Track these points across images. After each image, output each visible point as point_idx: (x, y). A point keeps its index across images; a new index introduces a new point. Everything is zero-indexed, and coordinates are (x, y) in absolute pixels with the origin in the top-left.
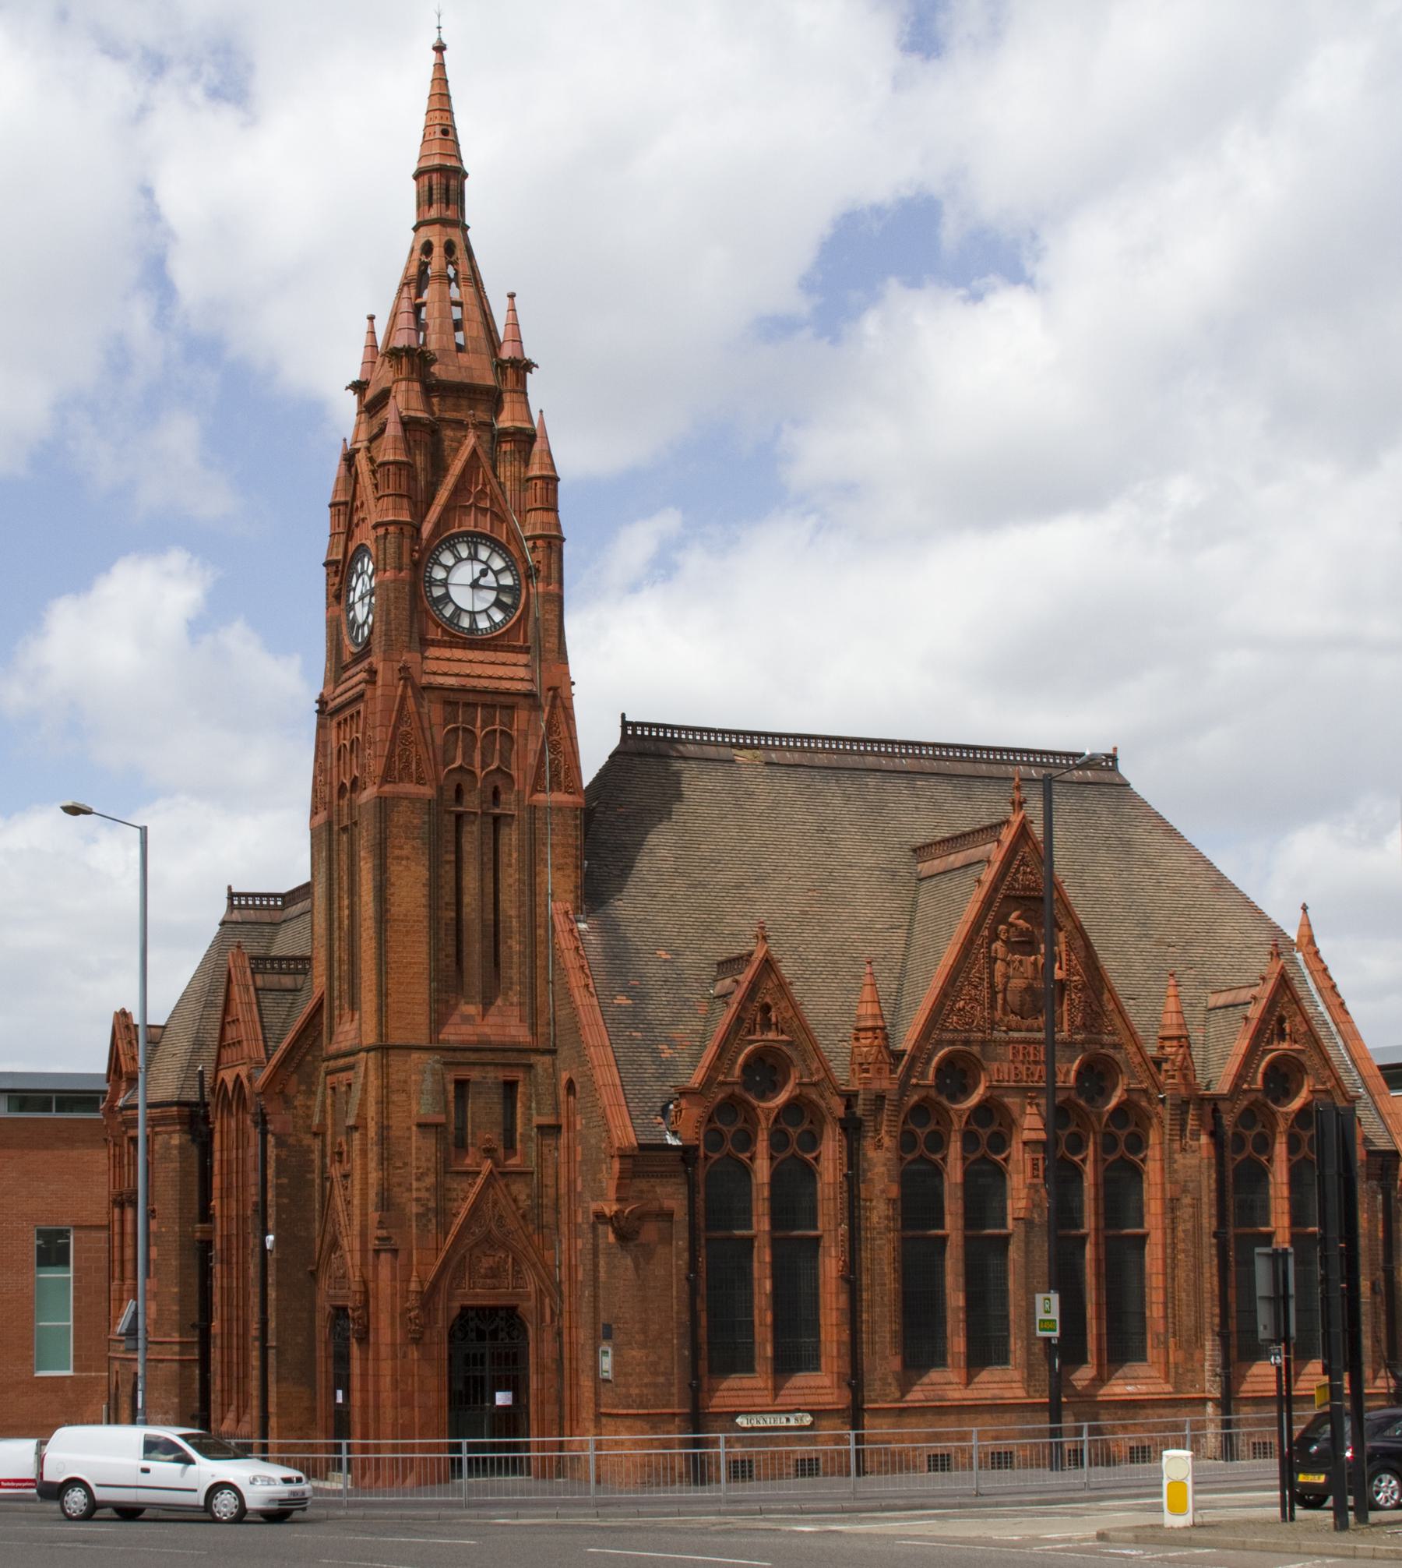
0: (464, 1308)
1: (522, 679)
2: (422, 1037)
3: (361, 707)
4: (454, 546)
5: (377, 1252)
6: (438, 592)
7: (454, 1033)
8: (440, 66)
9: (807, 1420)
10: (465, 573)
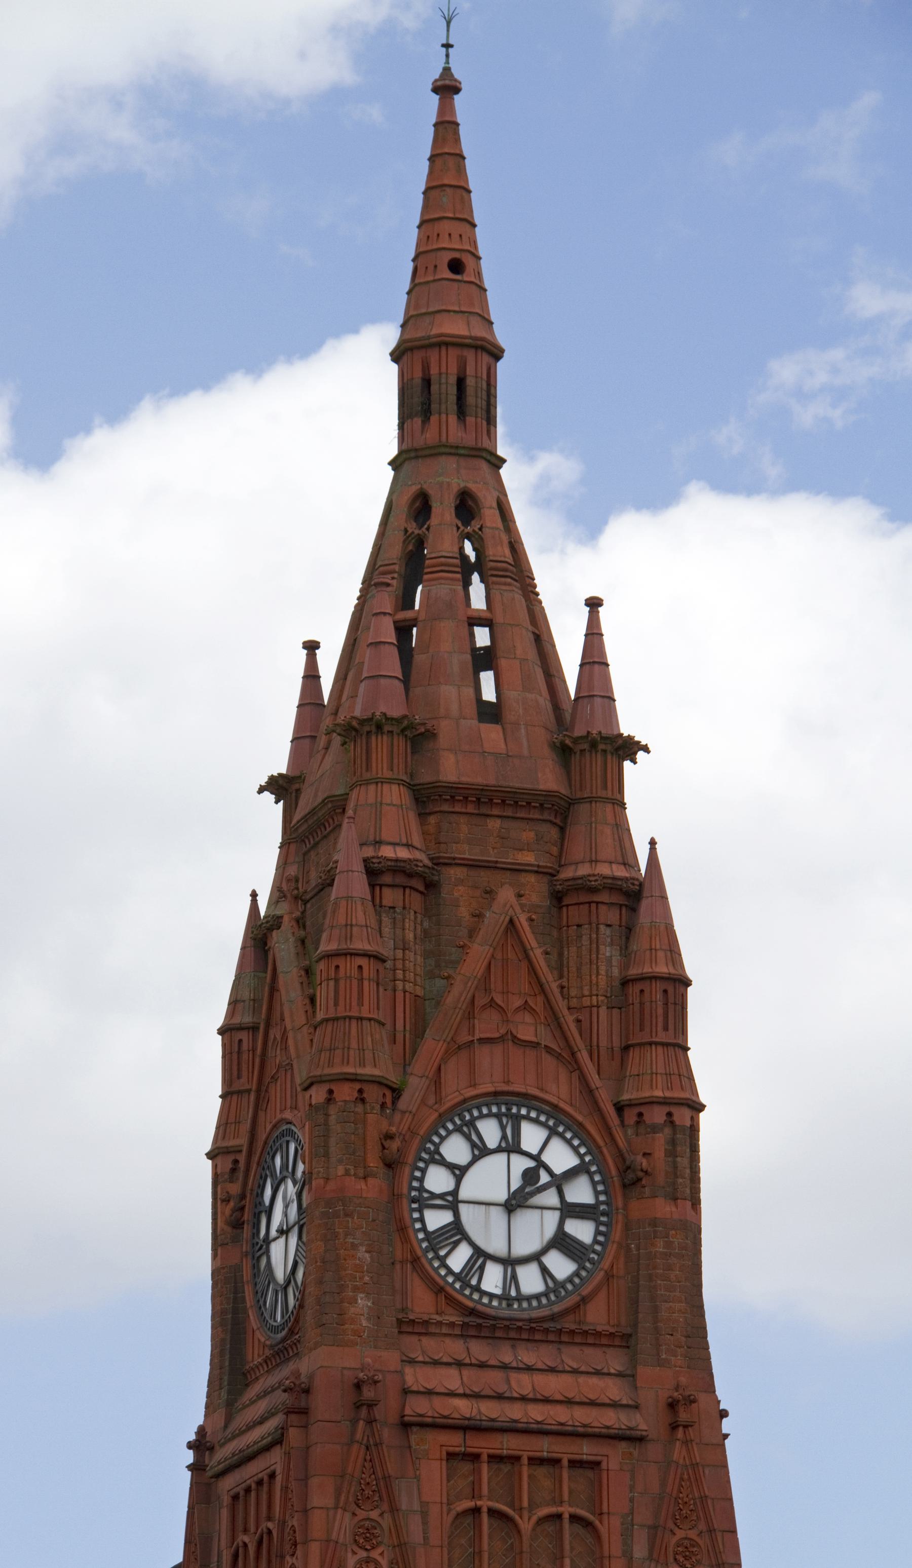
1: (614, 1405)
3: (275, 1459)
4: (472, 1124)
8: (446, 128)
10: (491, 1179)
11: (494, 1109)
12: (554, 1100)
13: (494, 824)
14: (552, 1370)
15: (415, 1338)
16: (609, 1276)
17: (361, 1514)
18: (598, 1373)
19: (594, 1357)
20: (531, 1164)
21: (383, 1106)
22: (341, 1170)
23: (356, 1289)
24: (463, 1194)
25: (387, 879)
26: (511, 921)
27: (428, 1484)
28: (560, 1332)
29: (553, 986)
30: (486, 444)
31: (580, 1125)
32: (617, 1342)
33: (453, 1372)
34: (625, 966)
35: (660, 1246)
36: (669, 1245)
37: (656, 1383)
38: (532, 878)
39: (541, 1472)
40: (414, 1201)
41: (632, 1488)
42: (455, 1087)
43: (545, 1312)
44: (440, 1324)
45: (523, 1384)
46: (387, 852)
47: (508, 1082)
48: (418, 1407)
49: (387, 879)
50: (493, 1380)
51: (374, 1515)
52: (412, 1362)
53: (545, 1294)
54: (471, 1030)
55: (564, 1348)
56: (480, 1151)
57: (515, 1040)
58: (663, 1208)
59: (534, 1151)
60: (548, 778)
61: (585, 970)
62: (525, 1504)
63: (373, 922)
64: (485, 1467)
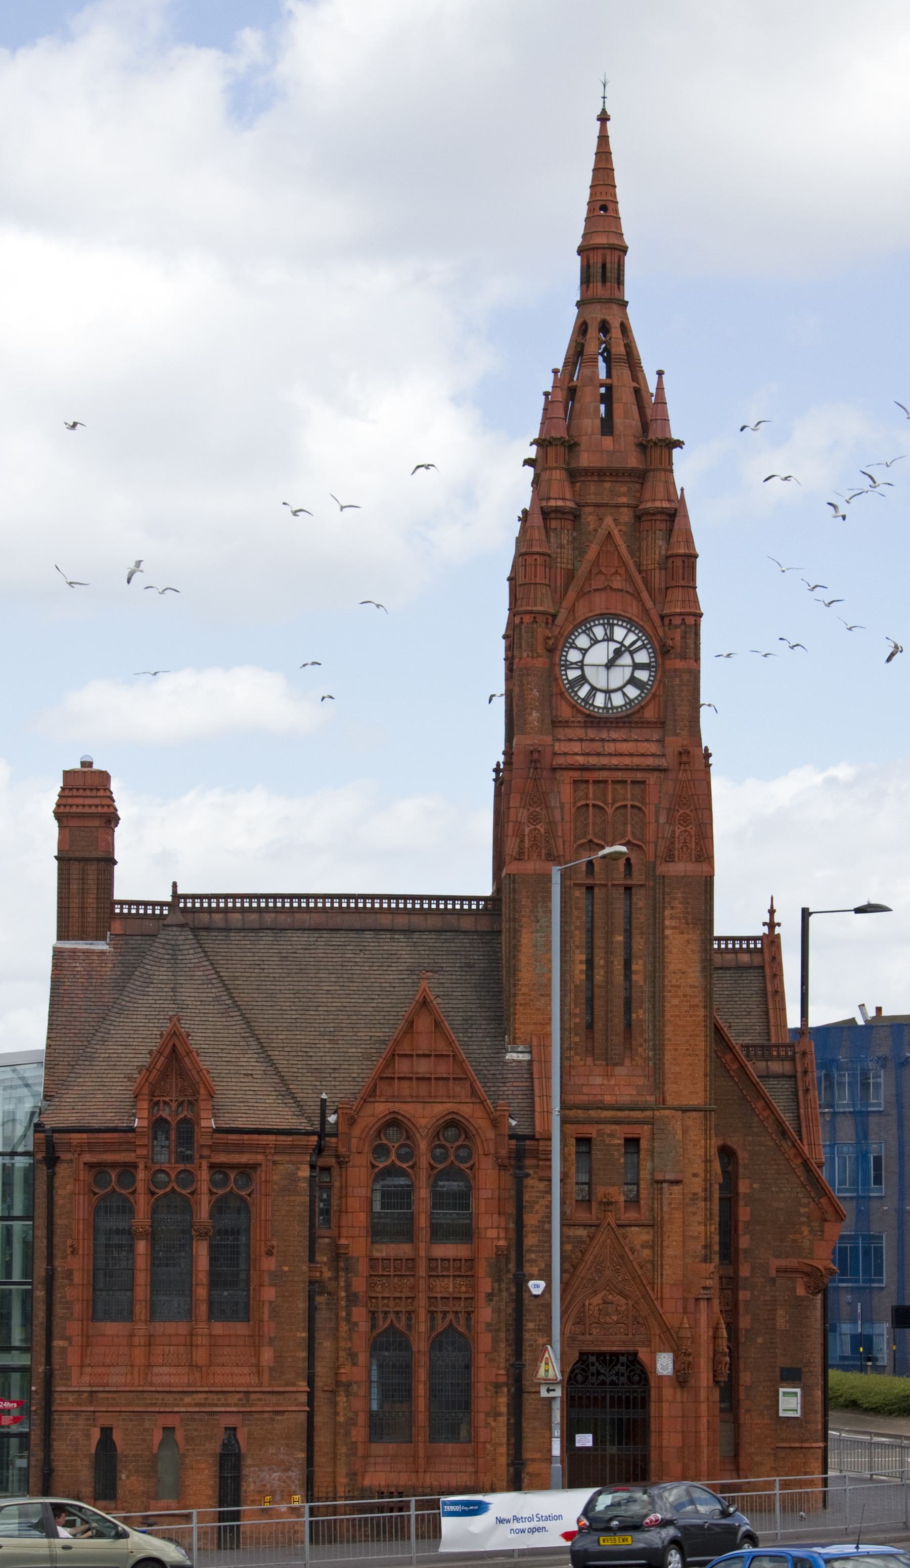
1: (653, 755)
4: (590, 629)
8: (603, 139)
10: (600, 654)
11: (601, 622)
12: (629, 615)
13: (607, 485)
14: (625, 740)
15: (561, 729)
16: (654, 696)
17: (532, 809)
18: (647, 740)
19: (646, 733)
20: (619, 646)
21: (547, 623)
22: (525, 655)
23: (532, 709)
24: (586, 662)
25: (553, 515)
26: (609, 533)
27: (564, 793)
28: (630, 722)
29: (630, 562)
30: (617, 295)
31: (642, 627)
32: (659, 725)
33: (578, 744)
34: (667, 551)
35: (677, 681)
36: (682, 680)
37: (674, 743)
38: (625, 510)
39: (618, 786)
40: (563, 666)
41: (660, 792)
42: (582, 611)
43: (624, 714)
44: (573, 722)
45: (610, 748)
46: (552, 503)
47: (607, 609)
48: (560, 761)
49: (553, 515)
50: (597, 747)
51: (538, 809)
52: (559, 740)
53: (625, 705)
54: (590, 586)
55: (633, 730)
56: (595, 642)
57: (611, 588)
59: (620, 640)
60: (633, 461)
61: (649, 552)
62: (610, 801)
63: (544, 537)
64: (591, 786)
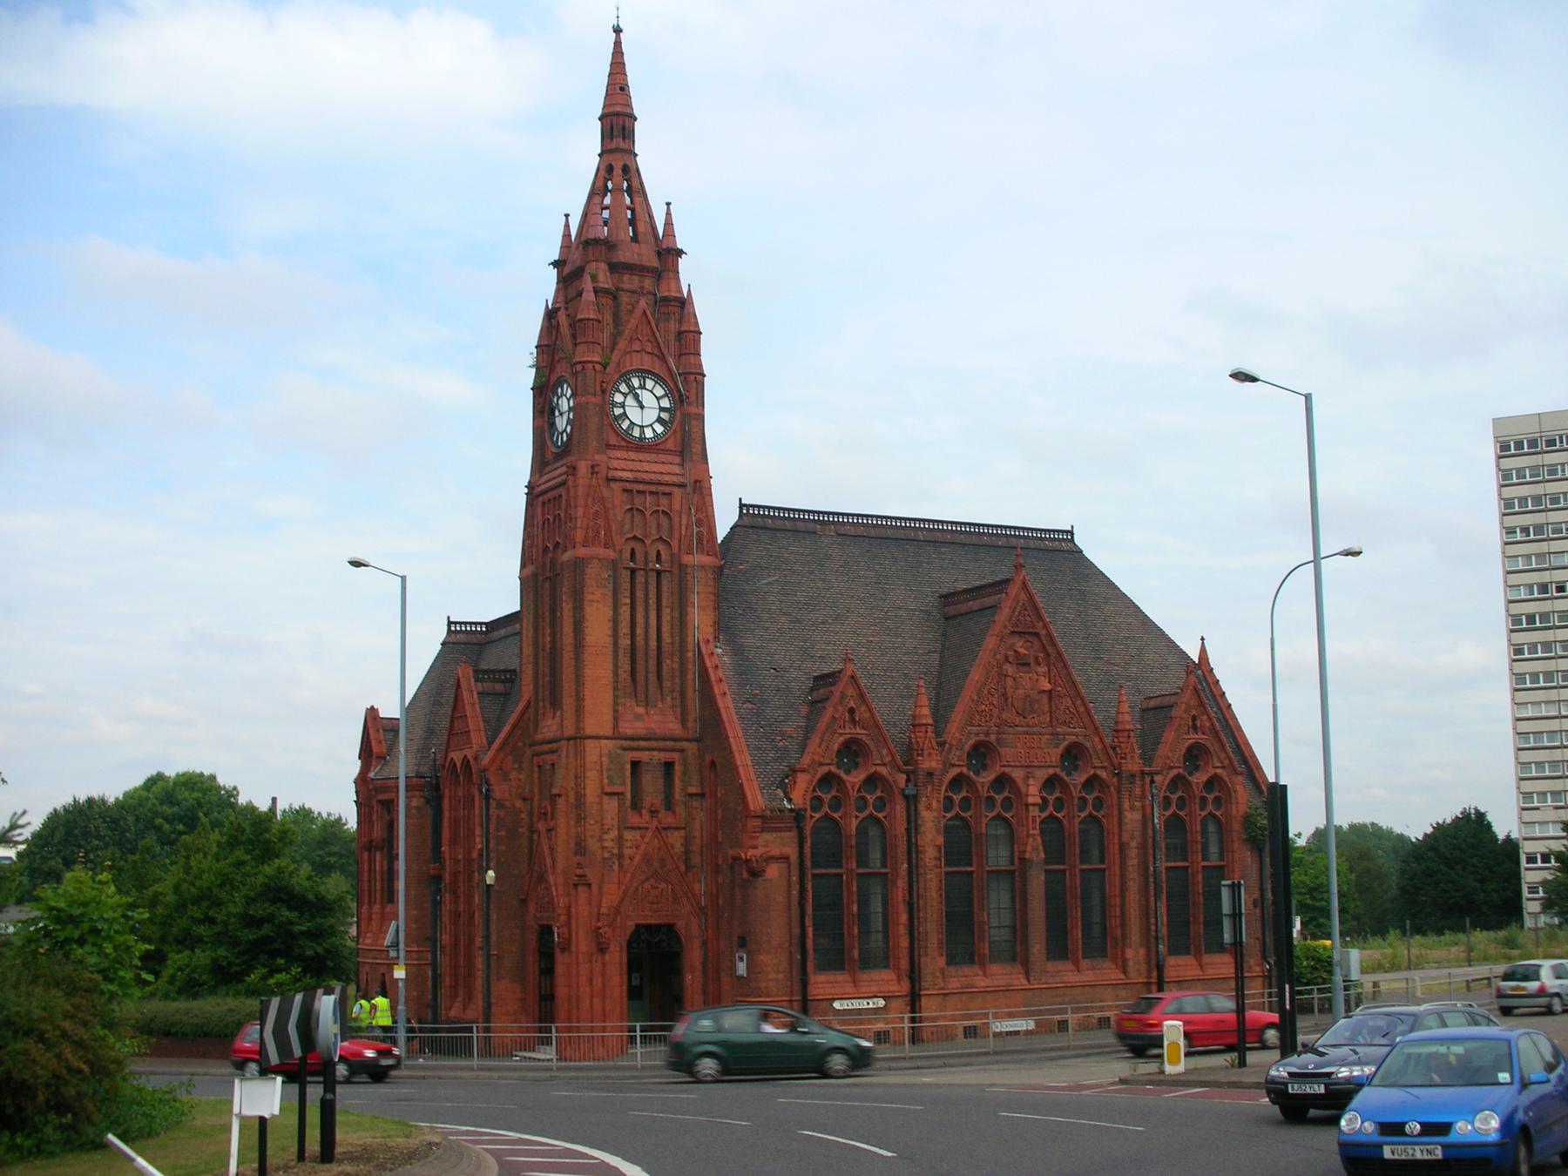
0: (637, 926)
2: (608, 731)
3: (562, 491)
5: (576, 885)
6: (618, 411)
7: (627, 728)
8: (618, 44)
9: (881, 1003)
19: (670, 458)
48: (612, 474)
58: (693, 410)
60: (654, 262)
